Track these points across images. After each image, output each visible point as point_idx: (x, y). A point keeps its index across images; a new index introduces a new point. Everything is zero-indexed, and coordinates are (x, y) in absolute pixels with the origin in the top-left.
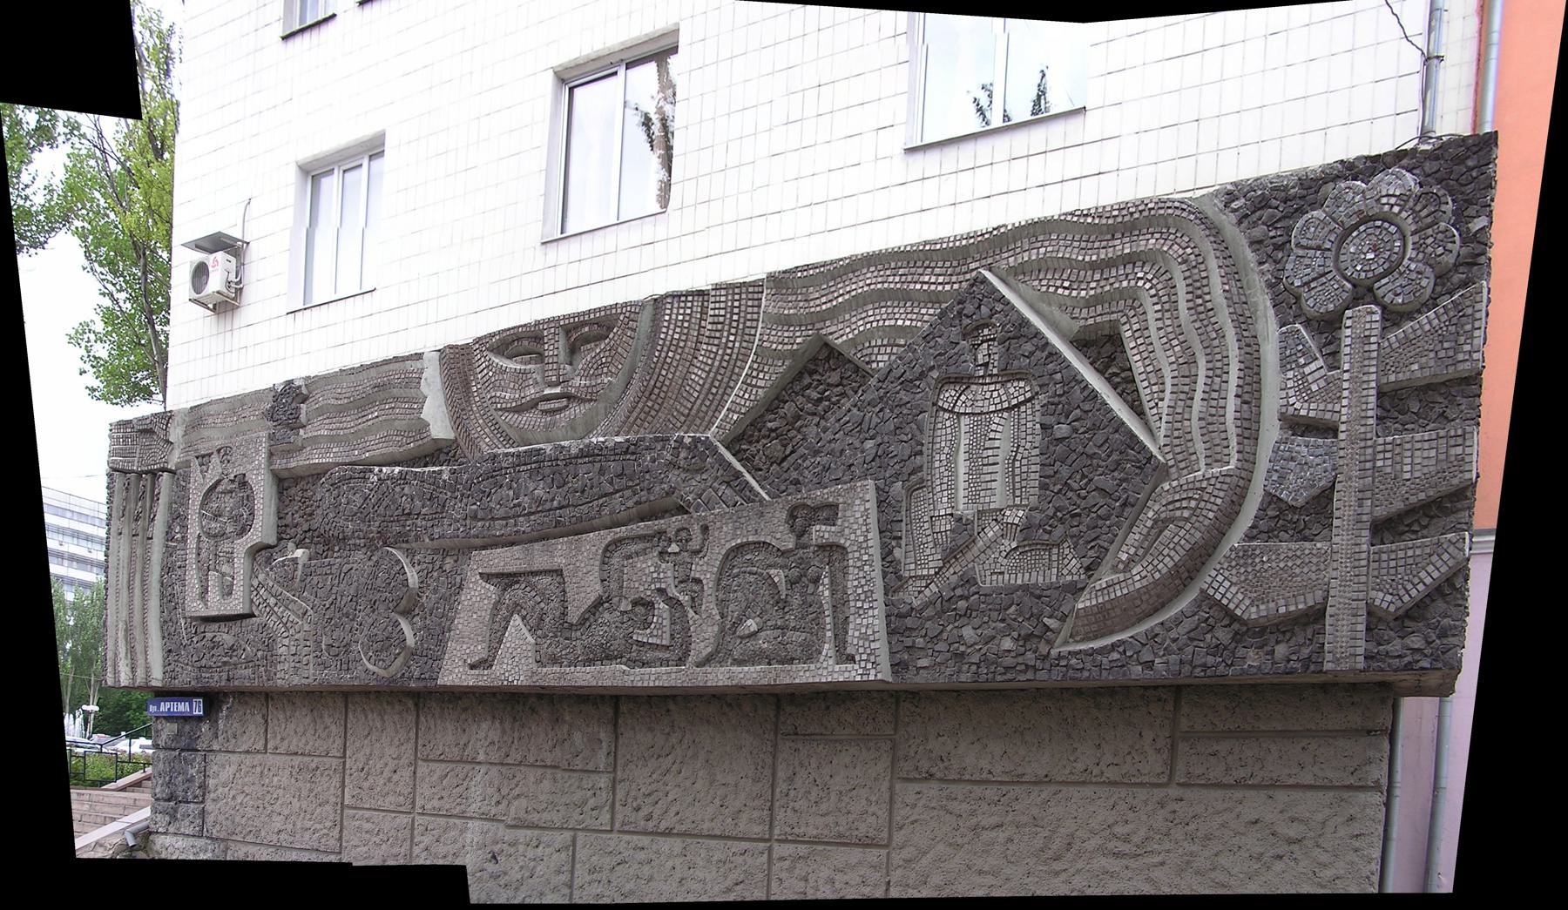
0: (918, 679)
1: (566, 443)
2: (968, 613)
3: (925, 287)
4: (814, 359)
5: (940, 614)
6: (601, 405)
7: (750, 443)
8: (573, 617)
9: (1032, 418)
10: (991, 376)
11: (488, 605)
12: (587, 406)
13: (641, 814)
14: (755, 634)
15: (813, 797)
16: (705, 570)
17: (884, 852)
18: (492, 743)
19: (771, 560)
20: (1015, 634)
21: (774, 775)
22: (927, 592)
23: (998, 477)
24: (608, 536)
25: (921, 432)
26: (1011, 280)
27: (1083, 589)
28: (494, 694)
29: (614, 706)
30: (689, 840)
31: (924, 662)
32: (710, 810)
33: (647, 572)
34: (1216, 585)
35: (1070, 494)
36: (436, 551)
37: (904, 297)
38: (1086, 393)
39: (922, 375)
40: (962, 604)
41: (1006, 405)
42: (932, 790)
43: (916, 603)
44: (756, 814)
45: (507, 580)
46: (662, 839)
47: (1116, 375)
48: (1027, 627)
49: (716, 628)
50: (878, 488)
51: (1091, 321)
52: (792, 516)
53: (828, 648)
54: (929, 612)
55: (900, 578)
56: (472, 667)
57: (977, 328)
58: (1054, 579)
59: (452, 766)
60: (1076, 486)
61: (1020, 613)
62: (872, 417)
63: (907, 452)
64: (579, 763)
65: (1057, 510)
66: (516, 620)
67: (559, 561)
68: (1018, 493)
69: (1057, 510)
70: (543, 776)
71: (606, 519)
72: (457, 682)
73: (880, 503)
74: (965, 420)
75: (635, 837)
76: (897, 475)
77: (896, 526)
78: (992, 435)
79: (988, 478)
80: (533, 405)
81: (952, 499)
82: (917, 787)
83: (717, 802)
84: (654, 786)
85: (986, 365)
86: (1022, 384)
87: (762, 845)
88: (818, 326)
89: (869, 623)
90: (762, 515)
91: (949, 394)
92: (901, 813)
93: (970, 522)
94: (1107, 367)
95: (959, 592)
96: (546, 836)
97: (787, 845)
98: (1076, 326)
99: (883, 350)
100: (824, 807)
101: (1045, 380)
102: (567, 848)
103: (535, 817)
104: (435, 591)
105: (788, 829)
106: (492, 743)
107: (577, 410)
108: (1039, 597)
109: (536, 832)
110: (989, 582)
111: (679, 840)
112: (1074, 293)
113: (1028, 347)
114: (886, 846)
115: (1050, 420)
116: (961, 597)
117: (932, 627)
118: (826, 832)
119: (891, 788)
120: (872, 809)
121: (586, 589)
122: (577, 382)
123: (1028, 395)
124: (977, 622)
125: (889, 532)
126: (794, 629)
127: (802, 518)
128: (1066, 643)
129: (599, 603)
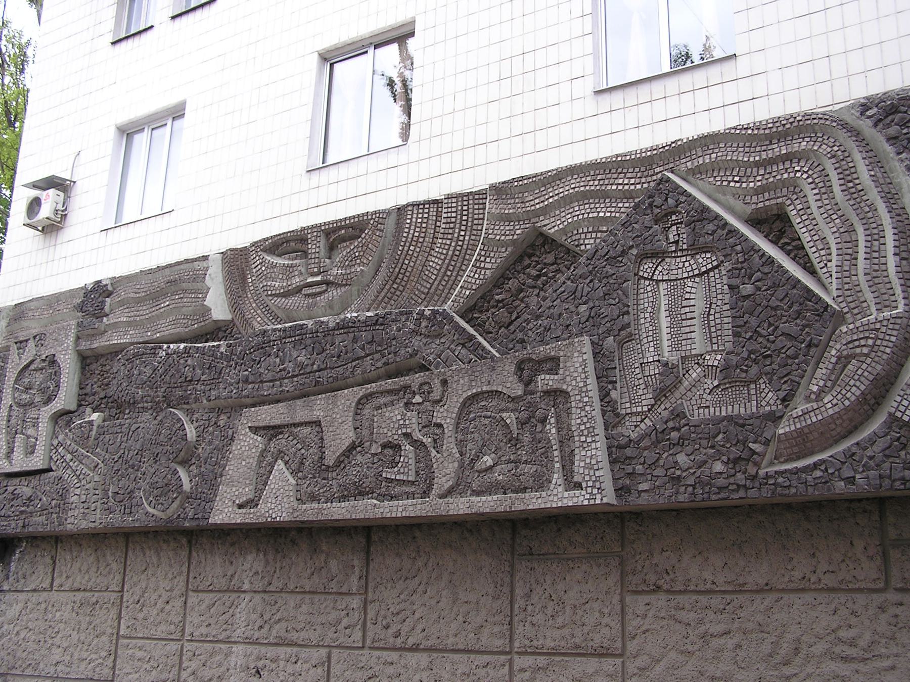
0: (640, 501)
1: (325, 319)
3: (620, 187)
4: (532, 246)
6: (355, 289)
7: (481, 312)
8: (330, 460)
9: (720, 281)
10: (682, 250)
11: (255, 453)
12: (343, 289)
13: (391, 631)
14: (491, 467)
15: (549, 611)
16: (446, 416)
17: (619, 661)
18: (257, 573)
19: (503, 405)
20: (725, 458)
21: (512, 592)
22: (643, 426)
23: (696, 328)
24: (360, 392)
26: (690, 178)
27: (781, 417)
28: (259, 530)
29: (366, 535)
30: (435, 655)
31: (644, 486)
32: (454, 626)
33: (394, 419)
35: (760, 339)
36: (212, 410)
37: (603, 195)
38: (764, 260)
39: (624, 253)
40: (674, 435)
41: (696, 272)
42: (660, 601)
43: (633, 436)
44: (496, 629)
45: (272, 431)
46: (409, 655)
48: (735, 452)
49: (456, 464)
50: (592, 343)
51: (761, 205)
52: (520, 368)
53: (557, 478)
54: (645, 443)
56: (240, 506)
57: (666, 215)
58: (754, 409)
59: (219, 595)
60: (764, 332)
62: (584, 287)
64: (334, 586)
65: (751, 352)
66: (280, 465)
67: (318, 414)
68: (714, 340)
69: (751, 352)
70: (302, 601)
71: (359, 378)
72: (226, 521)
73: (595, 355)
75: (385, 653)
76: (608, 332)
78: (687, 296)
79: (687, 329)
80: (298, 290)
81: (658, 348)
82: (646, 598)
83: (460, 618)
84: (402, 606)
85: (677, 242)
86: (709, 255)
87: (503, 658)
88: (533, 220)
89: (593, 455)
90: (493, 369)
91: (647, 267)
92: (633, 624)
93: (675, 366)
94: (779, 238)
95: (671, 424)
96: (304, 653)
97: (527, 657)
98: (749, 209)
99: (589, 236)
100: (560, 620)
101: (728, 251)
102: (323, 664)
103: (294, 636)
104: (210, 443)
105: (527, 642)
106: (257, 573)
107: (334, 293)
108: (743, 426)
109: (295, 649)
110: (697, 416)
111: (425, 655)
112: (744, 185)
113: (711, 227)
114: (621, 656)
115: (735, 282)
116: (673, 429)
118: (563, 643)
119: (622, 601)
120: (605, 620)
121: (341, 435)
122: (335, 271)
123: (715, 263)
124: (689, 449)
125: (605, 378)
126: (526, 462)
127: (527, 370)
128: (771, 464)
129: (352, 447)
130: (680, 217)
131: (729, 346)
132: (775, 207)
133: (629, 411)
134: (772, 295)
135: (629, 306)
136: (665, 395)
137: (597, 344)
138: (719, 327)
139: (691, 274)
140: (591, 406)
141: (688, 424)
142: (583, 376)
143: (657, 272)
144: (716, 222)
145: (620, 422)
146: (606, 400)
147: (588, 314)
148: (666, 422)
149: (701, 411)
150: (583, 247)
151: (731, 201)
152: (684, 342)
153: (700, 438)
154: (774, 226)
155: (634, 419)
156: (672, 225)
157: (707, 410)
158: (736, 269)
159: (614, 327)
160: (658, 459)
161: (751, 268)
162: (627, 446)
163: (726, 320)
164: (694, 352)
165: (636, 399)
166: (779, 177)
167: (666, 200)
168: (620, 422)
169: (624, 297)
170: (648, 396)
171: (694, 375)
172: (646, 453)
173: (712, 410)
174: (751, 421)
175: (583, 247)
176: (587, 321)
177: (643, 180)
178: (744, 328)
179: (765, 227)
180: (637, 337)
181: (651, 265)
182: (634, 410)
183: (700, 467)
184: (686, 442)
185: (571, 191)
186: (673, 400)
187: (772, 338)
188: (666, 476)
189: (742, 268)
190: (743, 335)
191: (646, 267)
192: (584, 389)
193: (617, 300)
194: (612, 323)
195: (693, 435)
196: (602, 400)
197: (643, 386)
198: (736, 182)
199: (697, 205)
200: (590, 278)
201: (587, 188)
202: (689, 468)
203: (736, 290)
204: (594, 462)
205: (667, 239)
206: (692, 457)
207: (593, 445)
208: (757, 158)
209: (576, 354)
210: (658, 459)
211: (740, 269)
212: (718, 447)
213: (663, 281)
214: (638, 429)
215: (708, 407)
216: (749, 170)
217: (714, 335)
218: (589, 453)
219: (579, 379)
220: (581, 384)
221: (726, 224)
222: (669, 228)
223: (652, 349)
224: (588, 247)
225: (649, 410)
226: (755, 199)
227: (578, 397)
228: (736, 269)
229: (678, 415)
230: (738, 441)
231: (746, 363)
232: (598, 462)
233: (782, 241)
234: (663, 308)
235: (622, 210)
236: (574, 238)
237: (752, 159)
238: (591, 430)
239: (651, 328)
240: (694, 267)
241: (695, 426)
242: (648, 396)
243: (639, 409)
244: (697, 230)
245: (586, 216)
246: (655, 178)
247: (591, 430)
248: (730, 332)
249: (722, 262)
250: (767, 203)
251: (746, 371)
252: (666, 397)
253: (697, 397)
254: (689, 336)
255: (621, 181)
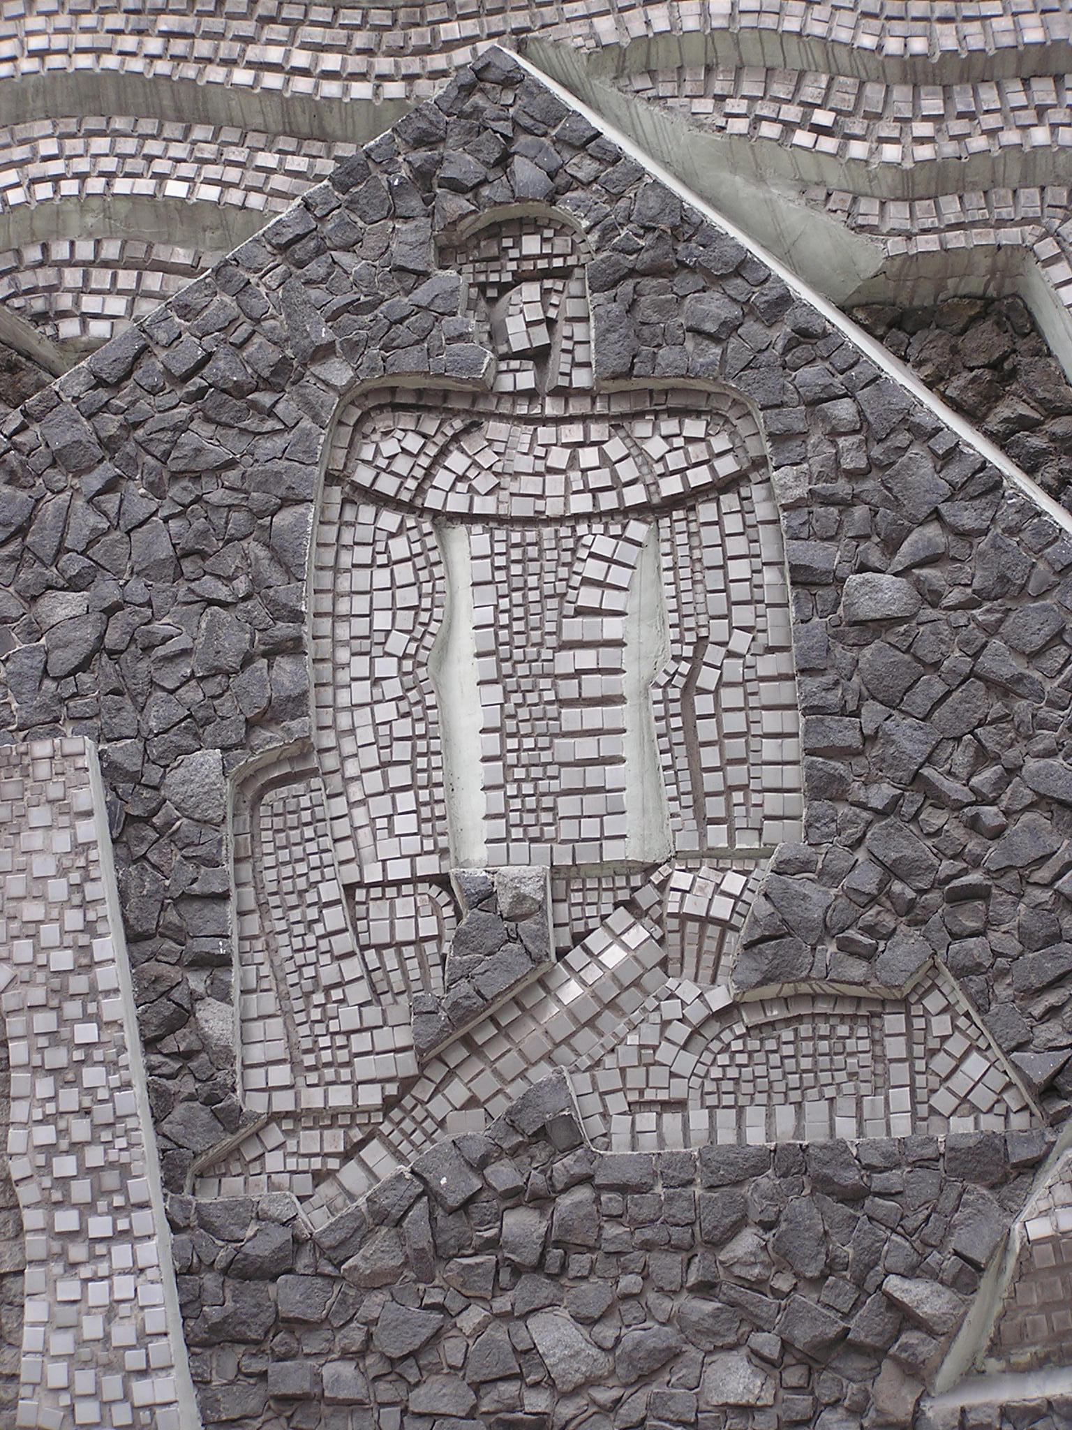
2: (552, 1262)
3: (272, 81)
5: (426, 1263)
9: (746, 549)
10: (563, 393)
20: (767, 1342)
22: (351, 1175)
23: (628, 746)
25: (292, 572)
26: (604, 87)
27: (1034, 1166)
34: (408, 1125)
35: (935, 818)
37: (186, 107)
38: (956, 472)
39: (280, 376)
40: (522, 1225)
41: (635, 496)
43: (316, 1221)
47: (1023, 424)
48: (814, 1320)
50: (111, 772)
51: (928, 243)
54: (377, 1253)
55: (230, 1119)
57: (494, 231)
58: (902, 1126)
60: (954, 788)
61: (783, 1259)
63: (234, 641)
65: (891, 871)
68: (715, 807)
69: (891, 871)
73: (124, 827)
74: (466, 545)
76: (197, 725)
77: (200, 918)
78: (588, 597)
79: (586, 748)
81: (435, 818)
85: (539, 356)
86: (695, 428)
91: (394, 449)
93: (525, 908)
94: (992, 398)
95: (504, 1175)
98: (870, 257)
99: (101, 278)
101: (794, 418)
108: (855, 1197)
110: (627, 1138)
112: (858, 149)
113: (713, 307)
115: (818, 555)
116: (515, 1197)
117: (397, 1319)
123: (726, 466)
124: (593, 1294)
128: (973, 1375)
130: (561, 245)
131: (787, 838)
132: (984, 263)
133: (284, 1102)
134: (991, 630)
135: (297, 617)
136: (467, 1041)
137: (135, 778)
138: (736, 748)
139: (608, 501)
140: (112, 1066)
141: (587, 1180)
142: (74, 919)
143: (442, 479)
144: (737, 286)
145: (235, 1153)
146: (170, 1044)
147: (89, 633)
148: (478, 1167)
149: (647, 1120)
150: (69, 328)
151: (792, 210)
152: (567, 805)
153: (647, 1246)
154: (969, 343)
155: (310, 1140)
156: (520, 278)
157: (672, 1121)
158: (828, 501)
159: (225, 706)
160: (437, 1335)
161: (896, 504)
162: (268, 1271)
163: (771, 722)
164: (613, 851)
165: (317, 1037)
166: (1011, 137)
167: (504, 161)
168: (235, 1153)
169: (274, 575)
170: (384, 1039)
171: (614, 957)
172: (373, 1304)
173: (699, 1119)
174: (894, 1179)
175: (69, 328)
176: (84, 665)
177: (384, 65)
178: (860, 764)
179: (931, 343)
180: (330, 761)
181: (413, 443)
182: (314, 1099)
183: (643, 1379)
184: (580, 1263)
185: (27, 65)
186: (509, 1065)
187: (991, 815)
188: (471, 1415)
189: (856, 499)
190: (857, 791)
191: (389, 447)
192: (78, 984)
193: (242, 585)
194: (212, 687)
195: (611, 1230)
196: (149, 1044)
197: (360, 992)
198: (820, 130)
199: (653, 202)
200: (107, 470)
201: (111, 62)
202: (592, 1381)
203: (827, 593)
204: (123, 1334)
205: (496, 334)
206: (607, 1332)
207: (121, 1254)
208: (918, 46)
209: (40, 816)
210: (437, 1335)
211: (845, 504)
212: (730, 1291)
213: (469, 518)
214: (327, 1190)
215: (678, 1105)
216: (874, 92)
217: (712, 782)
218: (98, 1293)
219: (49, 934)
220: (63, 960)
221: (785, 300)
222: (504, 288)
223: (405, 824)
224: (99, 329)
225: (389, 1104)
226: (898, 214)
227: (45, 1021)
228: (828, 501)
229: (542, 1134)
230: (831, 1267)
231: (870, 915)
232: (144, 1338)
233: (1004, 411)
234: (465, 641)
235: (278, 182)
236: (26, 280)
237: (893, 46)
238: (111, 1180)
239: (403, 728)
240: (627, 471)
241: (622, 1189)
242: (384, 1039)
243: (340, 1097)
244: (645, 310)
245: (96, 185)
246: (438, 61)
247: (111, 1180)
248: (793, 776)
249: (759, 463)
250: (956, 240)
251: (869, 955)
252: (475, 1050)
253: (627, 1056)
254: (593, 776)
255: (274, 54)
